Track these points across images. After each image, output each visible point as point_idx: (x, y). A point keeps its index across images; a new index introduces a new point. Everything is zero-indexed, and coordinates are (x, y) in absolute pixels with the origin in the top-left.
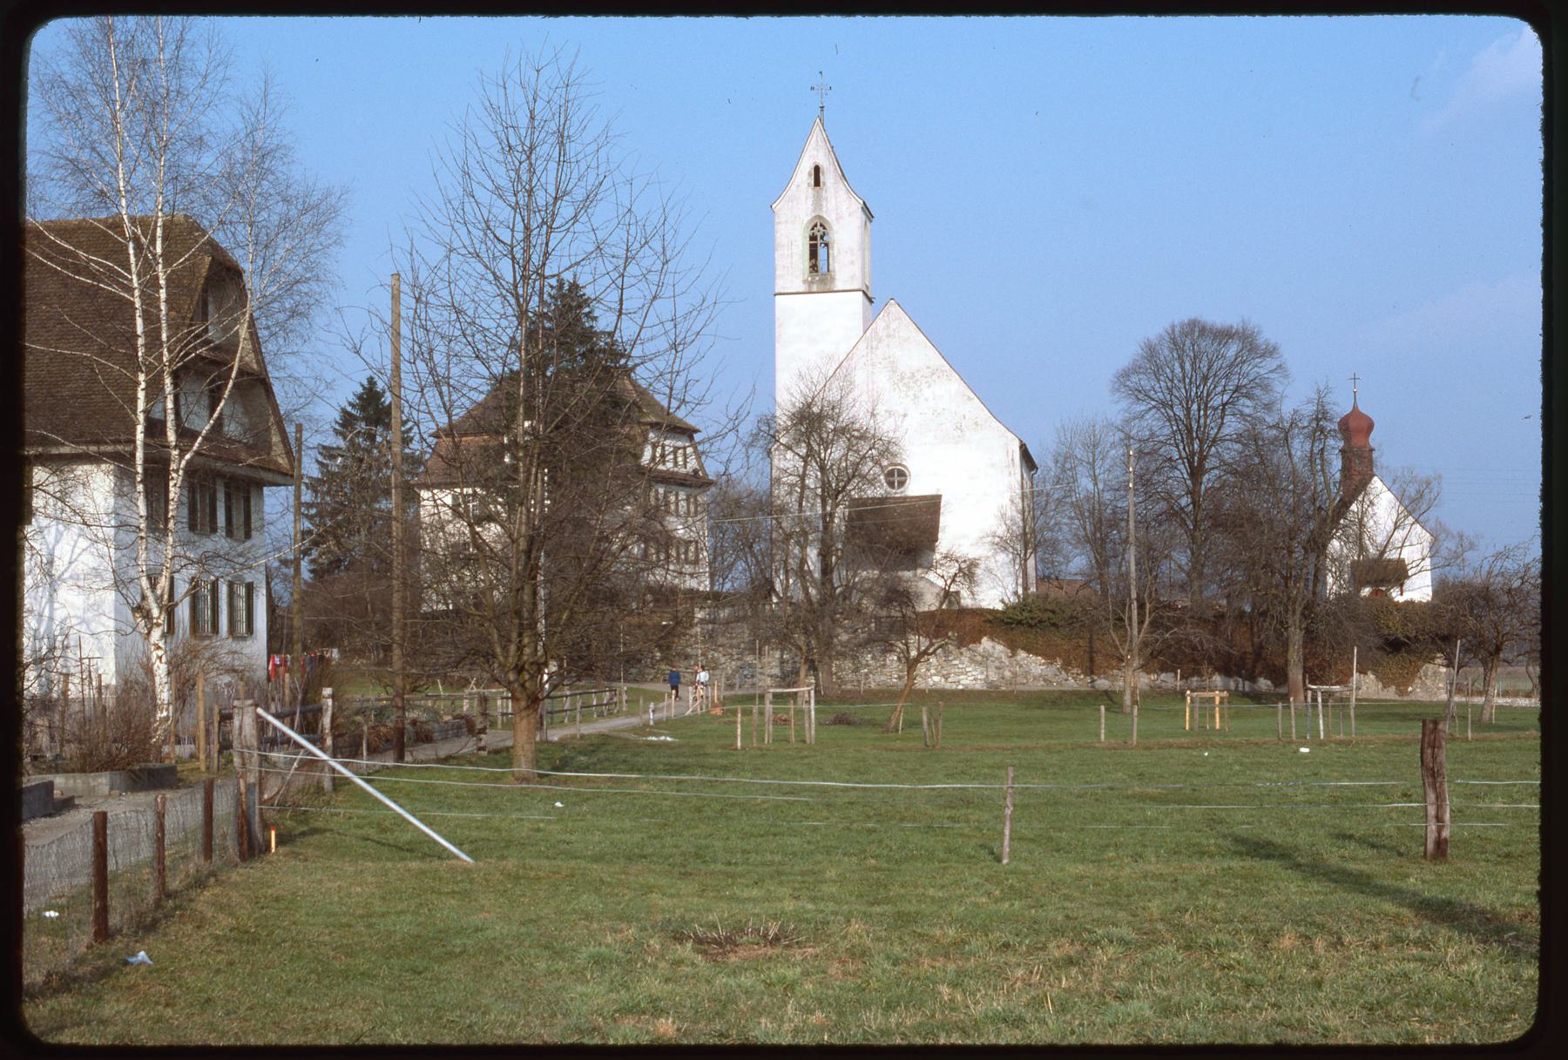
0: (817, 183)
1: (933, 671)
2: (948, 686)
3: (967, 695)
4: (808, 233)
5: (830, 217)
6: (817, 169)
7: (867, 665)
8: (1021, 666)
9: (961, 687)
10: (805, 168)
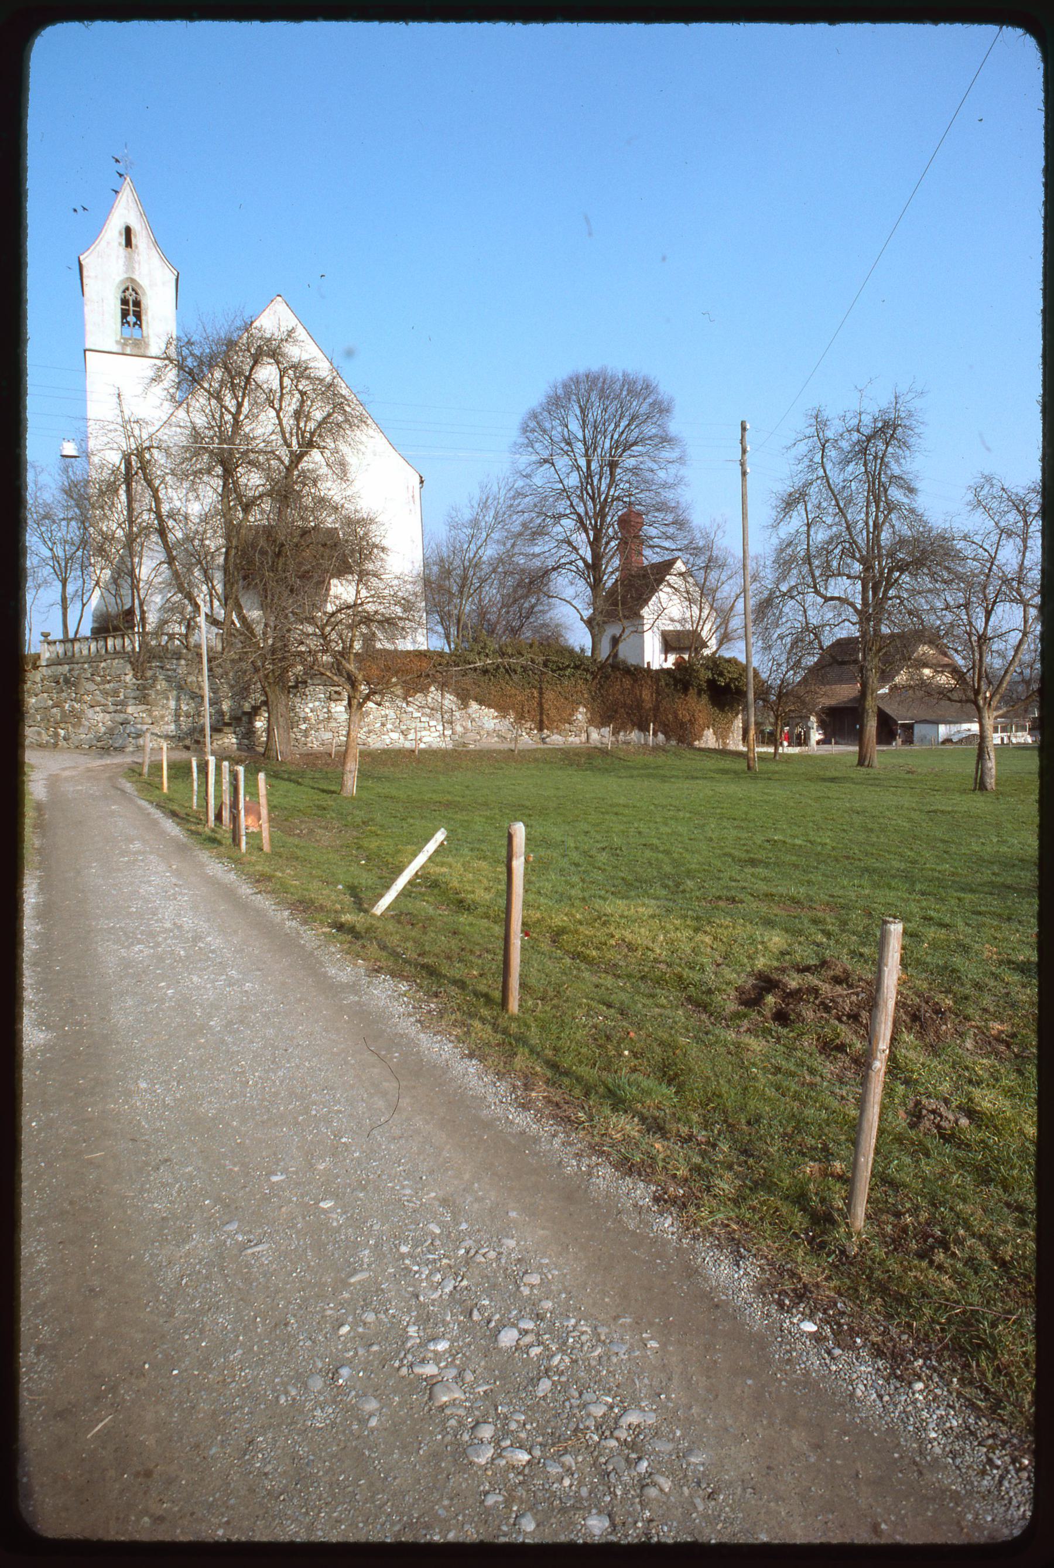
0: (129, 243)
1: (389, 726)
2: (408, 745)
3: (432, 754)
4: (119, 295)
5: (143, 281)
6: (128, 231)
7: (306, 719)
8: (473, 720)
9: (422, 746)
10: (113, 232)
